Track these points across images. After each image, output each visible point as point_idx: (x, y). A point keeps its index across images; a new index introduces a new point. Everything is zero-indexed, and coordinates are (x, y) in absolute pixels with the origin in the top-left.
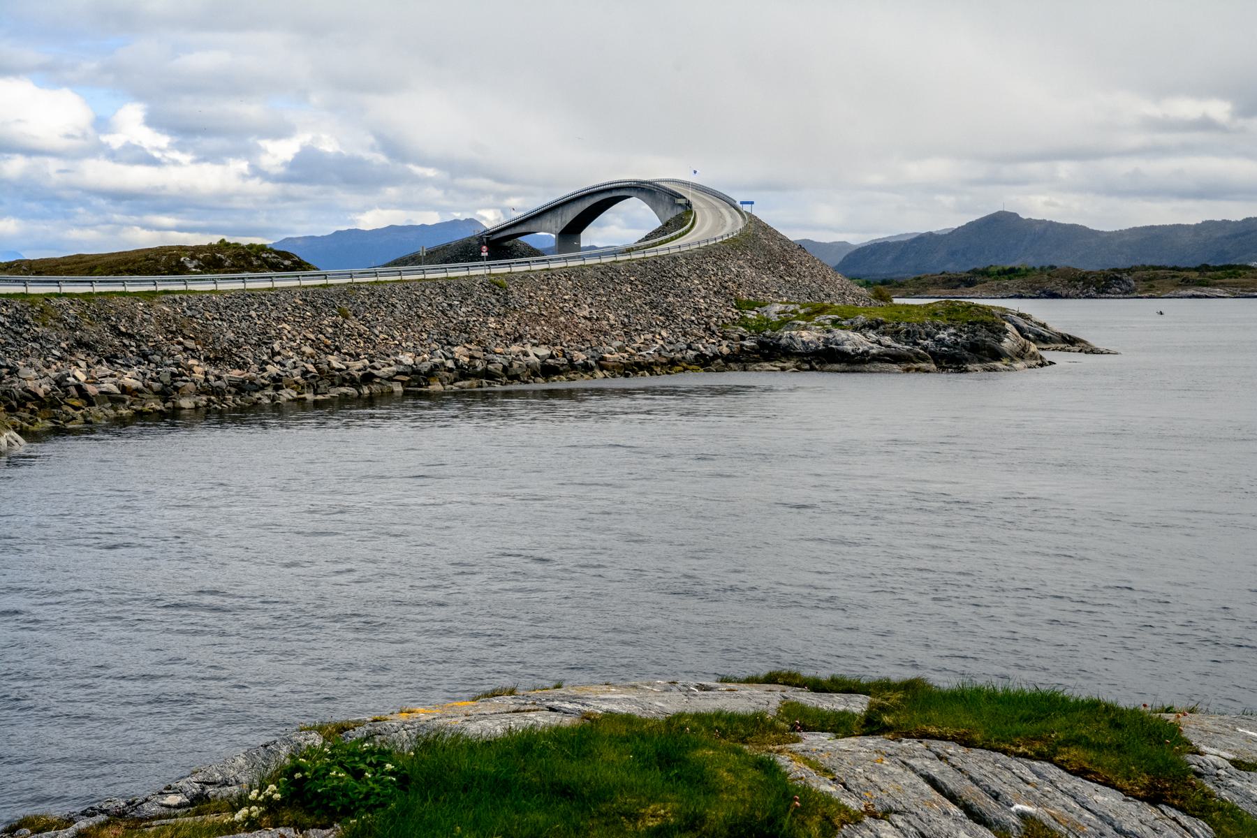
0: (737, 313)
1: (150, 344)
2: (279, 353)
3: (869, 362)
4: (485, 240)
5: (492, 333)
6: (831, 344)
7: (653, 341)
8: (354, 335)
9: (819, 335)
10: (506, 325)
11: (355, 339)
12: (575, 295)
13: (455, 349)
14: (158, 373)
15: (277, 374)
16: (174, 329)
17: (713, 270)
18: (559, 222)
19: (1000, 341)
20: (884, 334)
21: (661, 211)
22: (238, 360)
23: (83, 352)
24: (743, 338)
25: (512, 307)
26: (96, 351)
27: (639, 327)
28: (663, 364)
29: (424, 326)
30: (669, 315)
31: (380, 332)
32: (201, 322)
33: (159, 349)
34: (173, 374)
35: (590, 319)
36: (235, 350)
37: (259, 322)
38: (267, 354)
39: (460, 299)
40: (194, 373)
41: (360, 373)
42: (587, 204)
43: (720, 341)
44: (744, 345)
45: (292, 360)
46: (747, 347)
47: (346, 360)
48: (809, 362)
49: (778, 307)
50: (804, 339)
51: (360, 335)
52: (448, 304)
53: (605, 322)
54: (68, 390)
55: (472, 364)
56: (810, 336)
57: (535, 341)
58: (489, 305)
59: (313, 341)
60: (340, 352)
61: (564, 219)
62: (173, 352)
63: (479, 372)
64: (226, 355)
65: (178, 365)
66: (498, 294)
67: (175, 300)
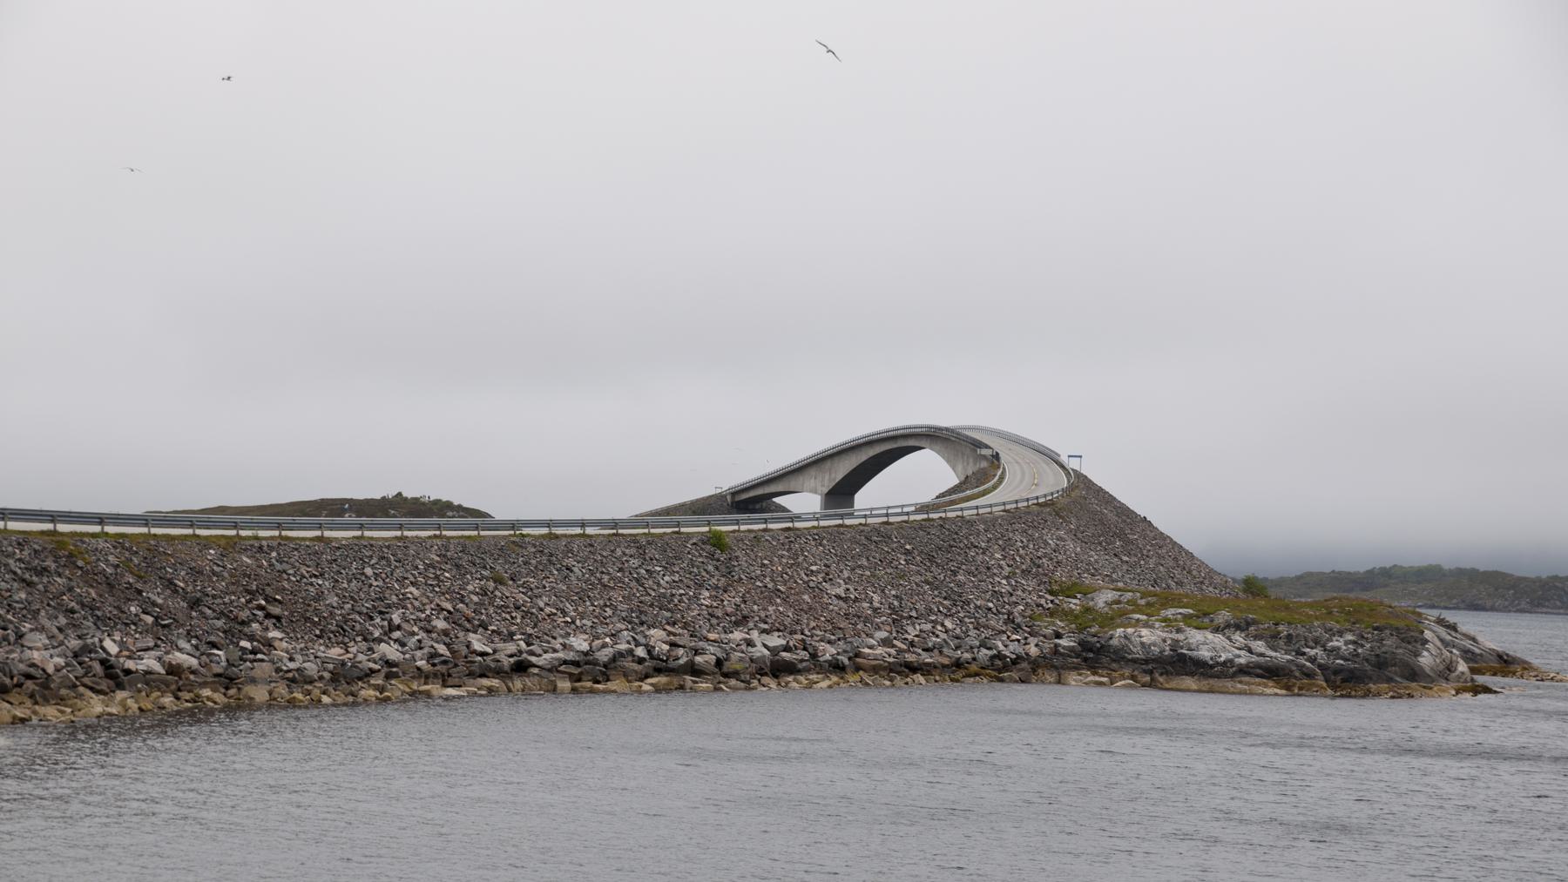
3: (1233, 676)
9: (1165, 635)
12: (826, 565)
17: (1022, 542)
18: (827, 477)
19: (1417, 654)
20: (1256, 638)
24: (1058, 636)
30: (957, 600)
35: (845, 600)
39: (664, 563)
42: (863, 456)
45: (417, 637)
46: (1064, 648)
48: (1151, 672)
49: (1109, 596)
50: (1144, 640)
53: (866, 605)
56: (1150, 636)
59: (449, 612)
61: (833, 475)
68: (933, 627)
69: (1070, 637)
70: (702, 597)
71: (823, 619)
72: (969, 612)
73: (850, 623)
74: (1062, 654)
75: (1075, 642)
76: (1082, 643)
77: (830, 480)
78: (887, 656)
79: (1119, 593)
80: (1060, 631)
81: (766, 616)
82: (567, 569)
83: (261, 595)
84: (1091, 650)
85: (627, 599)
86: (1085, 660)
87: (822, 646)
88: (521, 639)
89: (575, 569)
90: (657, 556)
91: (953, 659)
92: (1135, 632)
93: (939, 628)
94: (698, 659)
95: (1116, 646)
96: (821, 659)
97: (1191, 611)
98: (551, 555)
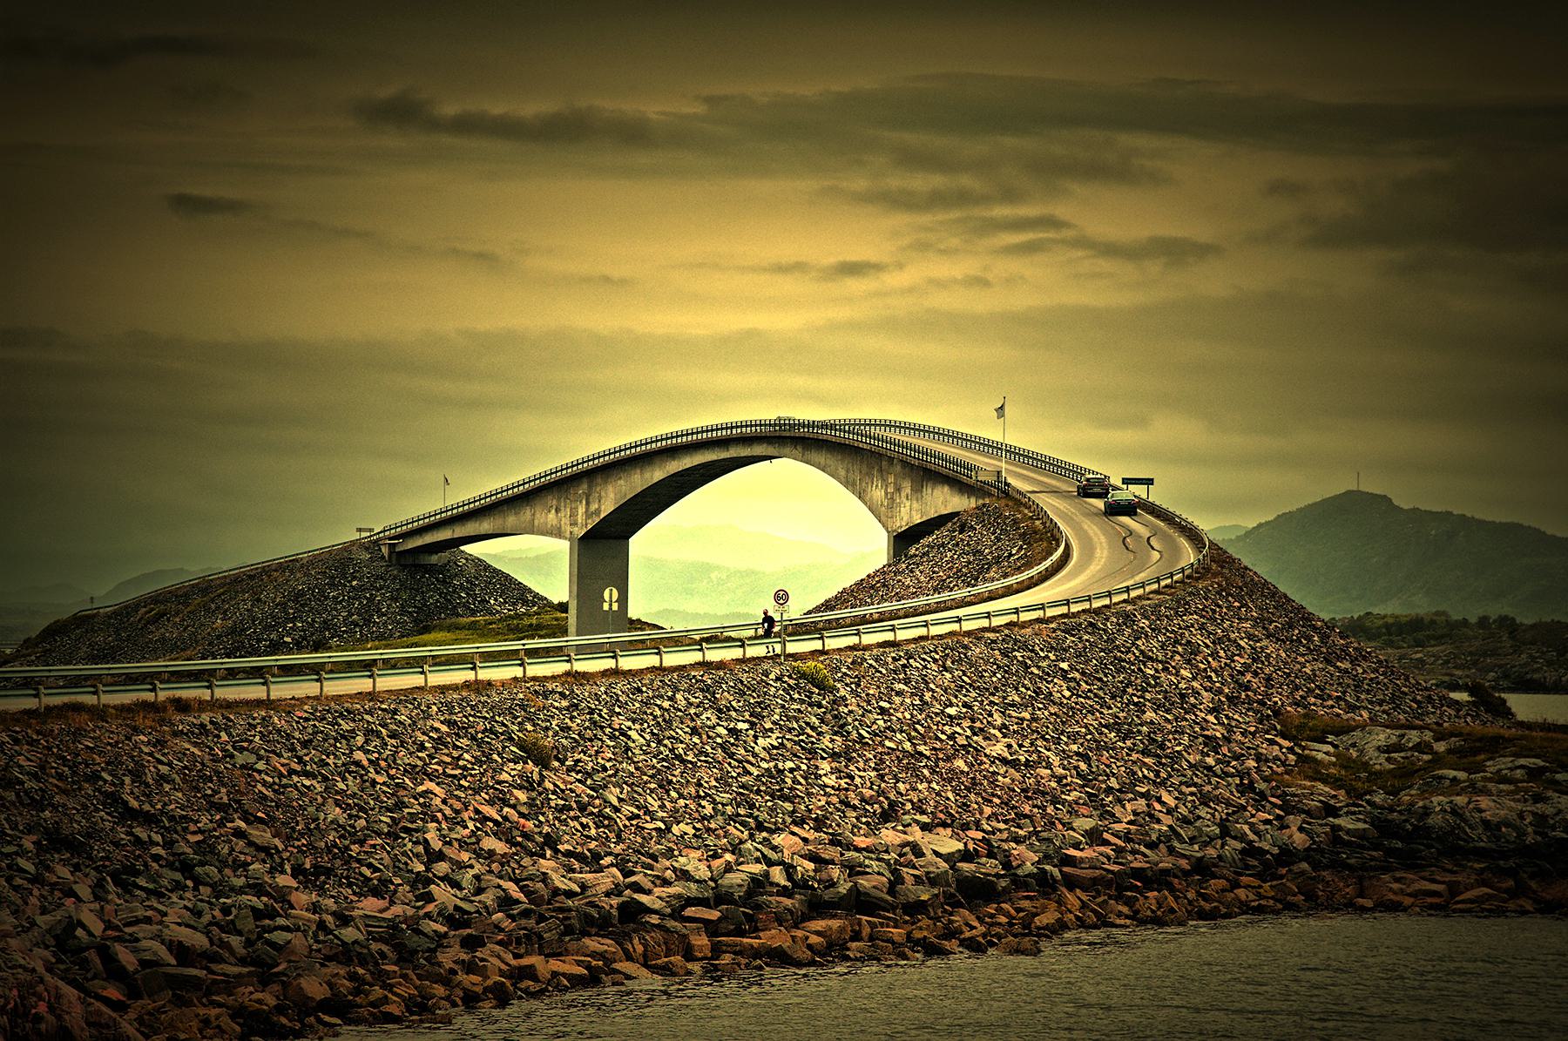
0: (1291, 750)
1: (193, 839)
2: (441, 856)
4: (385, 550)
5: (835, 800)
6: (1553, 828)
7: (1151, 816)
8: (571, 809)
9: (1520, 806)
10: (858, 781)
11: (576, 818)
12: (965, 705)
13: (778, 840)
14: (226, 910)
15: (457, 908)
16: (225, 800)
18: (581, 510)
21: (878, 494)
22: (367, 872)
23: (64, 862)
24: (1331, 811)
25: (854, 735)
26: (90, 858)
27: (1113, 783)
28: (1186, 873)
29: (699, 785)
31: (620, 800)
32: (270, 780)
33: (212, 850)
34: (257, 914)
35: (1014, 764)
36: (355, 848)
37: (380, 779)
38: (417, 855)
39: (747, 715)
40: (292, 907)
41: (615, 901)
42: (657, 474)
43: (1278, 817)
44: (1339, 828)
45: (472, 872)
46: (1348, 832)
47: (574, 871)
49: (1382, 737)
50: (1487, 815)
51: (582, 808)
52: (730, 730)
53: (1045, 772)
54: (86, 960)
55: (824, 876)
57: (924, 819)
58: (809, 731)
59: (496, 822)
60: (556, 851)
61: (594, 507)
62: (242, 857)
63: (843, 898)
64: (338, 862)
65: (258, 889)
66: (820, 706)
67: (203, 726)
68: (1148, 805)
69: (1354, 813)
70: (820, 772)
71: (996, 800)
72: (1185, 776)
73: (1034, 806)
74: (1348, 844)
75: (1365, 822)
76: (1375, 822)
77: (588, 515)
78: (1105, 860)
79: (1398, 732)
80: (1332, 802)
81: (920, 801)
82: (622, 734)
83: (236, 811)
84: (1396, 836)
85: (724, 781)
86: (1390, 852)
87: (1018, 850)
88: (612, 865)
89: (633, 734)
90: (734, 703)
91: (1193, 860)
92: (1469, 803)
93: (1157, 806)
94: (863, 882)
95: (1441, 828)
96: (1020, 872)
97: (1540, 762)
98: (592, 712)
